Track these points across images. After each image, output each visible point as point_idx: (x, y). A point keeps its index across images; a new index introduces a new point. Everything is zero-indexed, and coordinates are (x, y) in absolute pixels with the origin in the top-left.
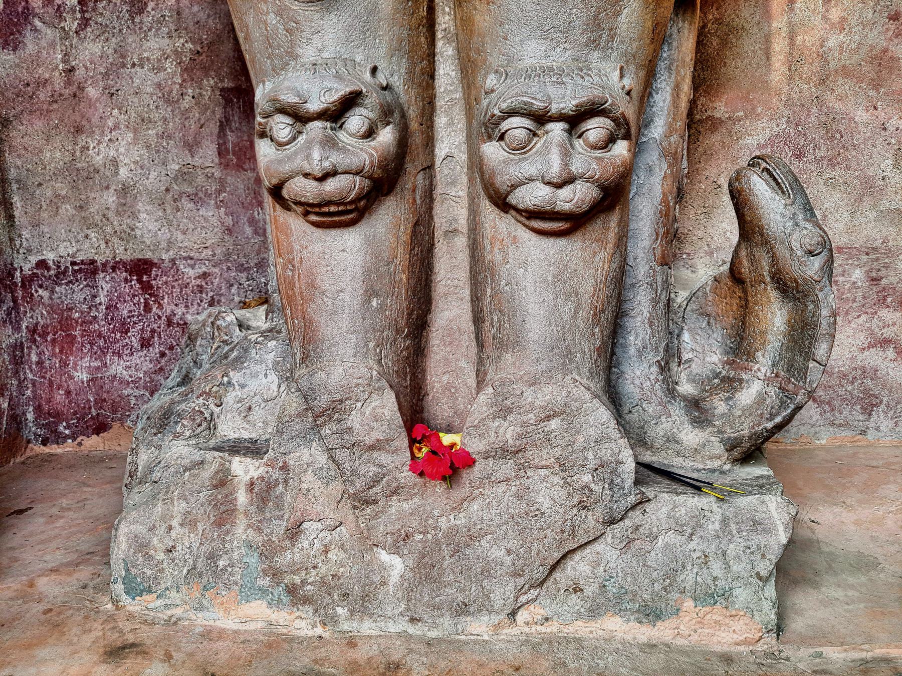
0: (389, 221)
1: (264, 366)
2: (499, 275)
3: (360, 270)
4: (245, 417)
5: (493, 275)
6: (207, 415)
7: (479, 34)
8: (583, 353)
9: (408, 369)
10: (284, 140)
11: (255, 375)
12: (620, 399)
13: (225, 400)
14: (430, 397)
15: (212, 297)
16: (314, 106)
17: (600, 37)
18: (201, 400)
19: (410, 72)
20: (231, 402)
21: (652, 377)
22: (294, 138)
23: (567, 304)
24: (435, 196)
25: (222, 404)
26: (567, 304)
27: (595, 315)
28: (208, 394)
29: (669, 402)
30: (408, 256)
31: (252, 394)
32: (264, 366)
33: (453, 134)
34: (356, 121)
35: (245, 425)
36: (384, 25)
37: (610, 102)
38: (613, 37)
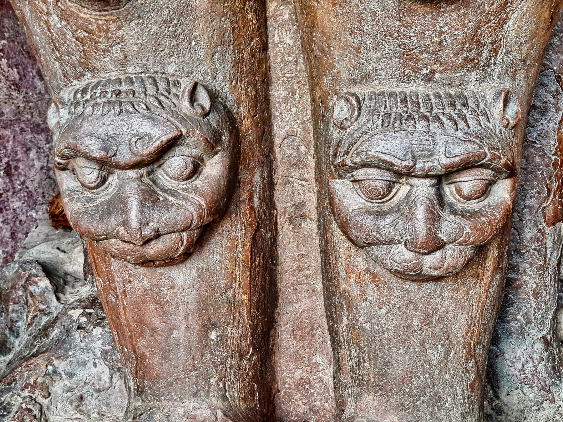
0: (228, 249)
1: (91, 354)
2: (357, 309)
3: (193, 306)
4: (78, 406)
5: (349, 306)
6: (36, 412)
7: (324, 33)
8: (455, 394)
9: (256, 386)
10: (92, 185)
11: (83, 364)
12: (498, 381)
13: (52, 390)
14: (282, 393)
15: (8, 163)
16: (124, 157)
17: (480, 54)
18: (26, 393)
19: (238, 64)
20: (60, 392)
21: (536, 356)
22: (104, 180)
23: (436, 348)
24: (275, 181)
25: (50, 394)
26: (436, 348)
27: (469, 351)
28: (34, 386)
29: (554, 383)
30: (248, 274)
31: (82, 383)
32: (91, 354)
33: (294, 110)
34: (176, 163)
35: (78, 415)
36: (200, 24)
37: (489, 156)
38: (496, 52)
